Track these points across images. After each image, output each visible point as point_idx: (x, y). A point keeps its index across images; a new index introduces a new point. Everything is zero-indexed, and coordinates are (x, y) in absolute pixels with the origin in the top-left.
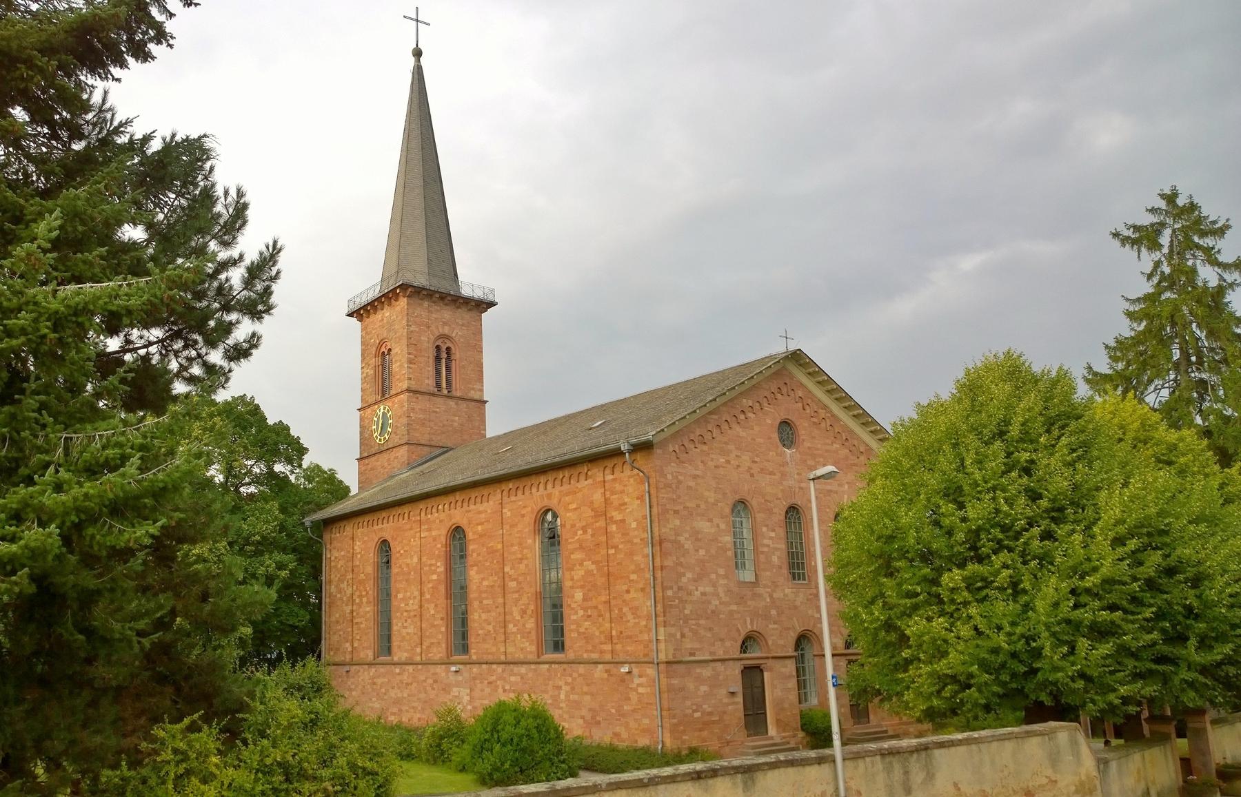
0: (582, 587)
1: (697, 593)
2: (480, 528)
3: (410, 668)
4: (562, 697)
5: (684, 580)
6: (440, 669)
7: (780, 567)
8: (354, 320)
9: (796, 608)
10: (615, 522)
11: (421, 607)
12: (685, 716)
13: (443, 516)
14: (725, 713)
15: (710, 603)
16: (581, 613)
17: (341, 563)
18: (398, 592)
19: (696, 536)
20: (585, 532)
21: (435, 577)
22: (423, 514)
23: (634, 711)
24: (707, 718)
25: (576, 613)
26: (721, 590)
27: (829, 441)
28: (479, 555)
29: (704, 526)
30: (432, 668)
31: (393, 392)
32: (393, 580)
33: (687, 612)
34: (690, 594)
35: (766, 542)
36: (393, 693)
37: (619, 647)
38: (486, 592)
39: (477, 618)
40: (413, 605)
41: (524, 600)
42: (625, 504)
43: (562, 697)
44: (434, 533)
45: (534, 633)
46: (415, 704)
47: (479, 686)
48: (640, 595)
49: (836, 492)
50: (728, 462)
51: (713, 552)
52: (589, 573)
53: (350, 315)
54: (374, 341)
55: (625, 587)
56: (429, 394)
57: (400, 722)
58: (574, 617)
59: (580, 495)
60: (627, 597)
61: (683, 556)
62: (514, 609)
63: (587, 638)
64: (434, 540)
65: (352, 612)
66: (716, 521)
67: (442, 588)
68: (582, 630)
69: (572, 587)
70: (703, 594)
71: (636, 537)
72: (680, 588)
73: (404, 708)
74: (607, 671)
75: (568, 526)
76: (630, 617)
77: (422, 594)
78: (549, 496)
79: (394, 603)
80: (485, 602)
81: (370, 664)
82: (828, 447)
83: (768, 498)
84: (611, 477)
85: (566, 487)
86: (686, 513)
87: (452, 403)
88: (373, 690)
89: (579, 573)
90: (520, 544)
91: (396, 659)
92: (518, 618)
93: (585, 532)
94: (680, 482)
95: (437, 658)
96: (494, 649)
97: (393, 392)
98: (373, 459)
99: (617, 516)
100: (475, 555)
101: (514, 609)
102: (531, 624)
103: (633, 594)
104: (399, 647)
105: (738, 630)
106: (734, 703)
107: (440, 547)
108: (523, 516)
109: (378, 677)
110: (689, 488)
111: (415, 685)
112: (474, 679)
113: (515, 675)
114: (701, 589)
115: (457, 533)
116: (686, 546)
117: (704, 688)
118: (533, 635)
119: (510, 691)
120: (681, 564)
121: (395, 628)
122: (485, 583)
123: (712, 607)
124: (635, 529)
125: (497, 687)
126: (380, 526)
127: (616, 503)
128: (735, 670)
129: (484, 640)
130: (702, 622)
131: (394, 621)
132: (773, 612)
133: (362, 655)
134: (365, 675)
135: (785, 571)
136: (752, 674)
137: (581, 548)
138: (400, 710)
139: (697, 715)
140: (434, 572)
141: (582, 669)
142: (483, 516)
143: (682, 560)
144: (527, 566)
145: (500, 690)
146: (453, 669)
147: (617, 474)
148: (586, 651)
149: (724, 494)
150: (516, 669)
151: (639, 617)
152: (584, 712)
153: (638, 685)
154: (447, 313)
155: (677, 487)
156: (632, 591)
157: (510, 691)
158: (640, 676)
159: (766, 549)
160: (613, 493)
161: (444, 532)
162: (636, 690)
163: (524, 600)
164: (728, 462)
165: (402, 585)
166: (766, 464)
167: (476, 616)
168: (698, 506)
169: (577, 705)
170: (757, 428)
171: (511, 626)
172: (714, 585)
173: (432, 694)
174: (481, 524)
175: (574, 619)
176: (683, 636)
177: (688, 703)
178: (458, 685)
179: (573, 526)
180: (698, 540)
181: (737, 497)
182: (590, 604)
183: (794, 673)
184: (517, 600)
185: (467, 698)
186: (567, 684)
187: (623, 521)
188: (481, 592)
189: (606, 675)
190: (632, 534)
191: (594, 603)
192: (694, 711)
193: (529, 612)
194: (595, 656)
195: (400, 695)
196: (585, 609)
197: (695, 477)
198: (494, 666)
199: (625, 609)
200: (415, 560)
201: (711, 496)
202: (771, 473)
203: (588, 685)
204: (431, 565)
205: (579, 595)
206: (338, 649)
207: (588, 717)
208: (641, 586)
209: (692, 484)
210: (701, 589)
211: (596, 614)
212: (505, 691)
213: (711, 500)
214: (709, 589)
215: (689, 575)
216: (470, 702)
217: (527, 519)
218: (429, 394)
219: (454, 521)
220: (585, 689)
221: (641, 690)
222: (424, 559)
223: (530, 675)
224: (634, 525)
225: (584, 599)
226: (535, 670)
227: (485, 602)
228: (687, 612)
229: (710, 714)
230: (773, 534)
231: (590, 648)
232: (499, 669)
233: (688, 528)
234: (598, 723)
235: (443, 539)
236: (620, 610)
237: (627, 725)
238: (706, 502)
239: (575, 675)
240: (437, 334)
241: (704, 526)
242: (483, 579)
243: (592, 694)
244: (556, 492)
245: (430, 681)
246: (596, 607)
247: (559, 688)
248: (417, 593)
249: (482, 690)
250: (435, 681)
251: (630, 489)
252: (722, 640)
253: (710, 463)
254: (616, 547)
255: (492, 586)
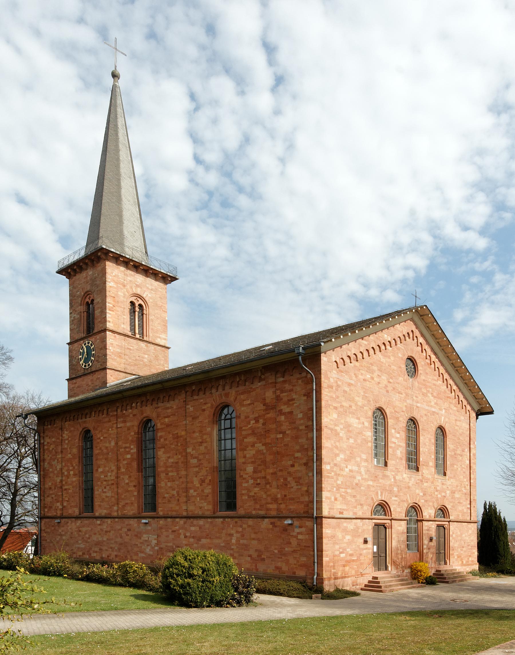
0: (253, 462)
1: (347, 470)
2: (167, 420)
3: (109, 521)
4: (234, 541)
5: (338, 459)
6: (133, 522)
7: (401, 459)
8: (63, 278)
9: (409, 487)
10: (284, 414)
11: (117, 477)
12: (334, 556)
13: (135, 411)
14: (361, 555)
15: (355, 477)
16: (251, 481)
17: (52, 447)
18: (99, 467)
19: (348, 427)
20: (257, 421)
21: (129, 456)
22: (119, 411)
23: (294, 551)
24: (349, 558)
25: (247, 482)
26: (363, 470)
27: (436, 378)
28: (165, 440)
29: (353, 421)
30: (127, 521)
31: (96, 331)
32: (94, 459)
33: (339, 482)
34: (341, 470)
35: (394, 440)
36: (95, 538)
37: (283, 506)
38: (171, 466)
39: (165, 487)
40: (111, 476)
41: (204, 472)
42: (293, 400)
43: (234, 541)
44: (128, 424)
45: (210, 496)
46: (113, 546)
47: (165, 533)
48: (303, 468)
49: (438, 414)
50: (372, 378)
51: (359, 441)
52: (259, 452)
53: (60, 272)
54: (80, 293)
55: (290, 463)
56: (125, 335)
57: (102, 558)
58: (246, 485)
59: (253, 394)
60: (292, 470)
61: (339, 441)
62: (195, 479)
63: (255, 499)
64: (129, 429)
65: (61, 481)
66: (362, 419)
67: (135, 464)
68: (252, 494)
69: (244, 463)
70: (351, 471)
71: (301, 425)
72: (335, 465)
73: (104, 548)
74: (271, 523)
75: (243, 417)
76: (293, 484)
77: (118, 468)
78: (227, 395)
79: (96, 475)
80: (170, 474)
81: (77, 518)
82: (435, 382)
83: (396, 409)
84: (281, 379)
85: (241, 388)
86: (341, 410)
87: (143, 345)
88: (79, 535)
89: (250, 453)
90: (201, 432)
91: (97, 514)
92: (198, 485)
93: (257, 421)
94: (338, 386)
95: (131, 513)
96: (177, 508)
97: (96, 331)
98: (79, 380)
99: (286, 409)
100: (162, 440)
101: (195, 479)
102: (208, 490)
103: (297, 467)
104: (100, 506)
105: (372, 499)
106: (366, 549)
107: (132, 435)
108: (204, 410)
109: (83, 526)
110: (345, 392)
111: (112, 532)
112: (161, 528)
113: (194, 526)
114: (349, 467)
115: (146, 424)
116: (341, 435)
117: (348, 537)
118: (210, 498)
119: (190, 537)
120: (337, 447)
121: (96, 493)
122: (171, 460)
123: (356, 481)
124: (301, 419)
125: (180, 534)
126: (84, 419)
127: (285, 399)
128: (369, 525)
129: (169, 501)
130: (349, 491)
131: (96, 488)
132: (395, 489)
133: (70, 511)
134: (73, 526)
135: (404, 462)
136: (381, 531)
137: (253, 433)
138: (101, 549)
139: (342, 555)
140: (128, 453)
141: (250, 522)
142: (169, 411)
143: (338, 444)
144: (206, 447)
145: (182, 536)
146: (144, 521)
147: (287, 377)
148: (255, 509)
149: (369, 401)
150: (195, 522)
151: (301, 484)
152: (252, 552)
153: (298, 533)
154: (140, 278)
155: (337, 390)
156: (296, 465)
157: (190, 537)
158: (300, 527)
159: (393, 445)
160: (282, 392)
161: (136, 423)
162: (296, 537)
163: (204, 472)
164: (372, 378)
165: (103, 462)
166: (397, 385)
167: (163, 484)
168: (351, 406)
169: (246, 547)
170: (392, 358)
171: (192, 491)
172: (359, 466)
173: (127, 539)
174: (168, 417)
175: (245, 488)
176: (336, 499)
177: (337, 547)
178: (147, 532)
179: (247, 417)
180: (349, 431)
181: (378, 406)
182: (259, 475)
183: (405, 531)
184: (198, 472)
185: (154, 542)
186: (237, 532)
187: (291, 413)
188: (167, 467)
189: (271, 526)
190: (298, 422)
191: (263, 474)
192: (341, 553)
193: (207, 481)
194: (262, 513)
195: (100, 539)
196: (255, 479)
197: (350, 385)
198: (177, 520)
199: (289, 479)
200: (113, 444)
201: (360, 401)
202: (400, 393)
203: (256, 533)
204: (126, 448)
205: (250, 469)
206: (51, 507)
207: (255, 555)
208: (304, 461)
209: (347, 389)
210: (349, 467)
211: (263, 482)
212: (186, 537)
213: (360, 404)
214: (355, 468)
215: (342, 456)
216: (157, 544)
217: (207, 413)
218: (125, 335)
219: (145, 415)
220: (253, 536)
221: (300, 537)
222: (120, 443)
223: (207, 526)
224: (300, 416)
225: (255, 472)
226: (211, 522)
227: (170, 474)
228: (339, 482)
229: (351, 555)
230: (398, 435)
231: (258, 506)
232: (182, 522)
233: (343, 421)
234: (263, 560)
235: (136, 429)
236: (285, 479)
237: (287, 562)
238: (356, 405)
239: (245, 526)
240: (131, 292)
241: (353, 421)
242: (169, 457)
243: (258, 539)
244: (233, 392)
245: (126, 530)
246: (265, 478)
247: (231, 535)
248: (114, 468)
249: (167, 536)
250: (129, 530)
251: (298, 389)
252: (361, 505)
253: (360, 376)
254: (284, 433)
255: (177, 463)
